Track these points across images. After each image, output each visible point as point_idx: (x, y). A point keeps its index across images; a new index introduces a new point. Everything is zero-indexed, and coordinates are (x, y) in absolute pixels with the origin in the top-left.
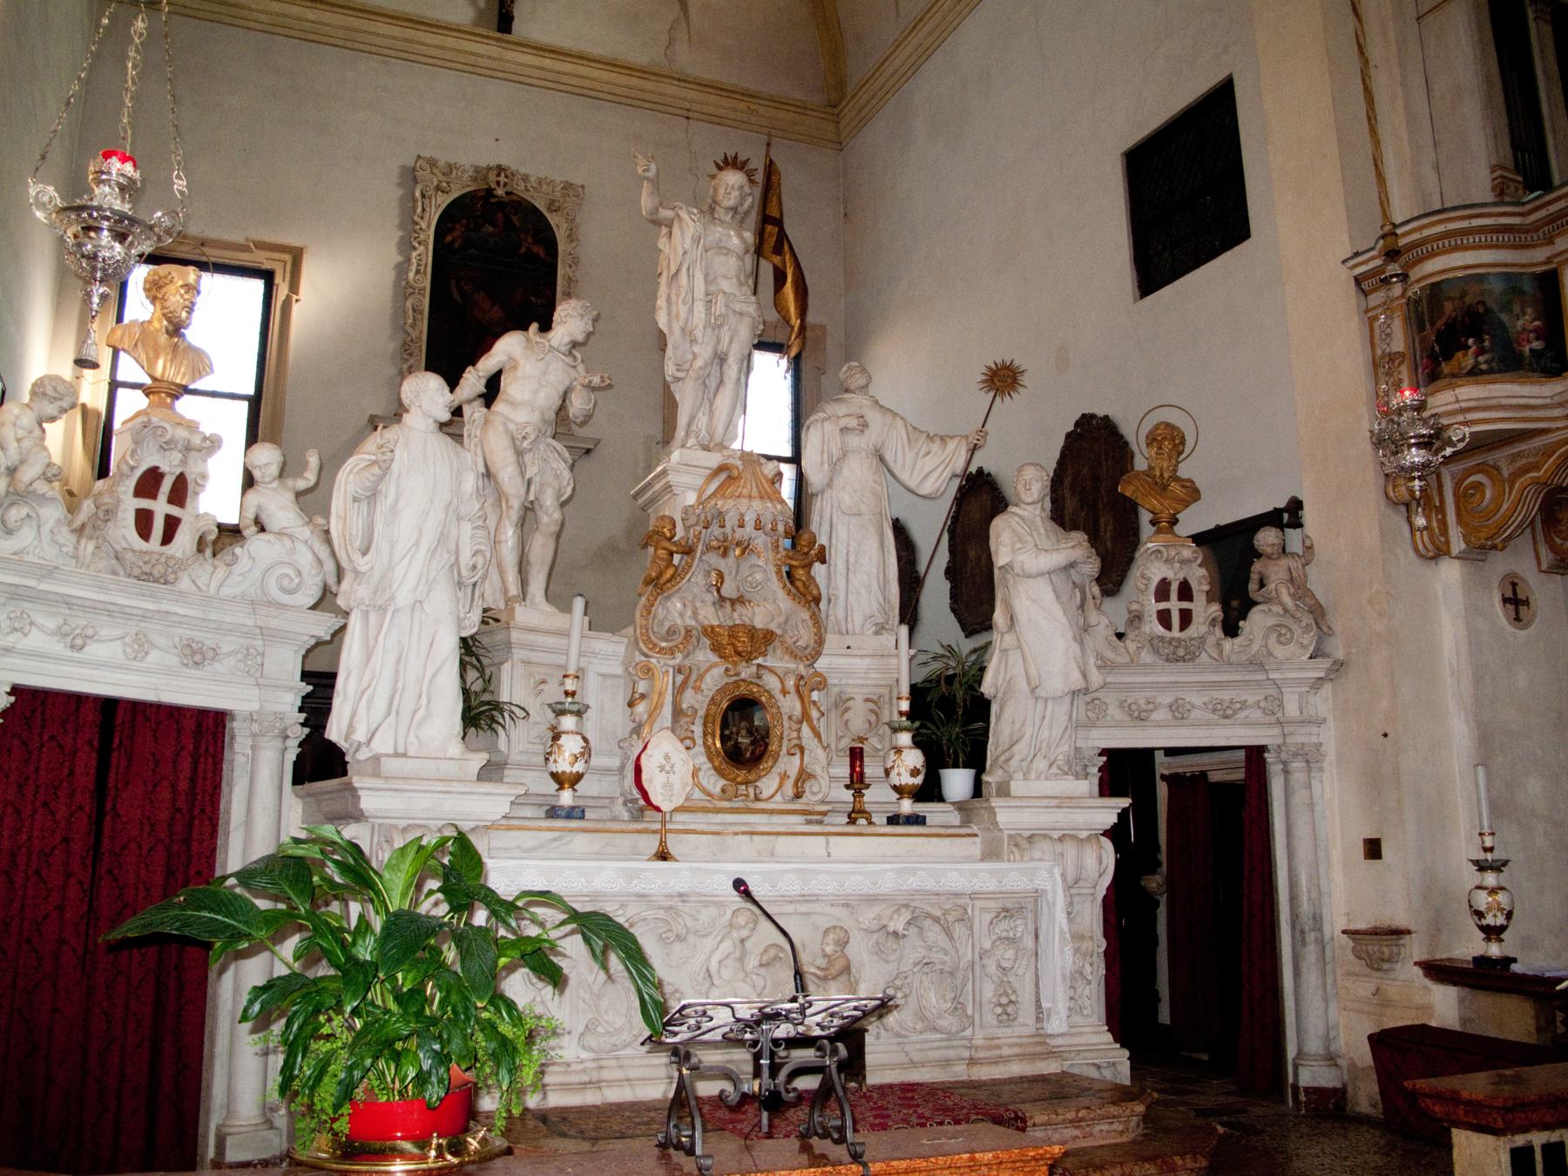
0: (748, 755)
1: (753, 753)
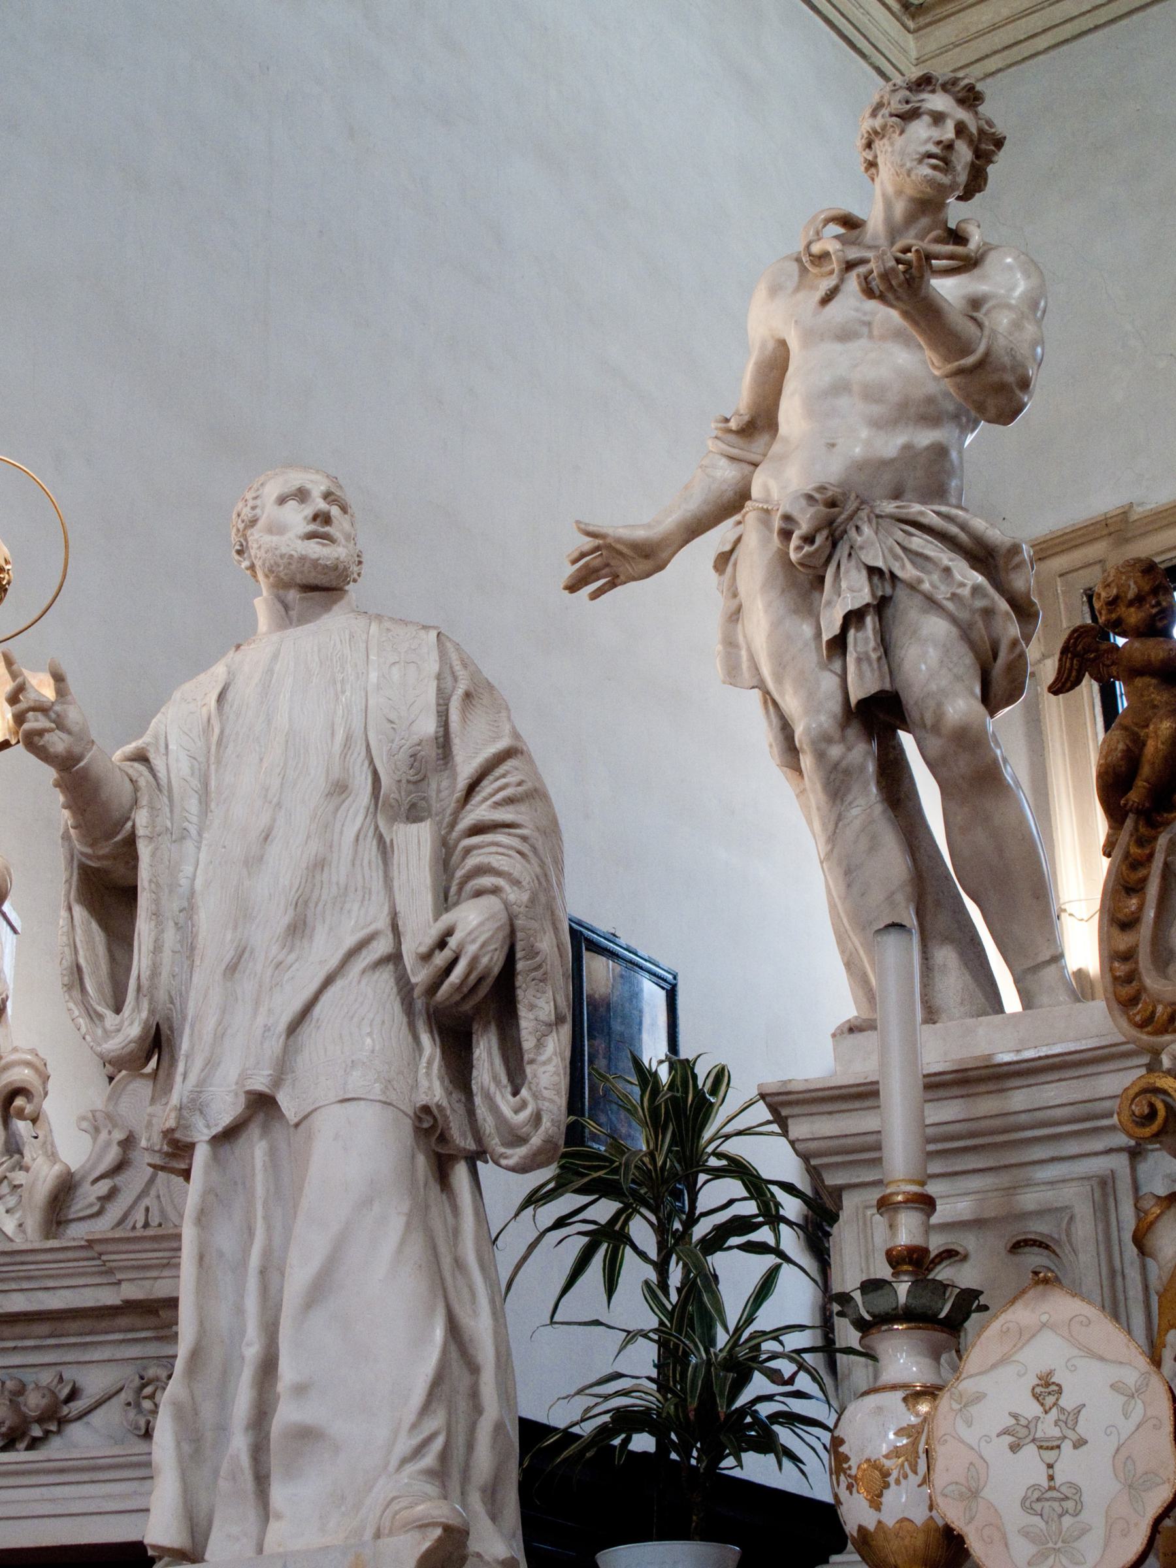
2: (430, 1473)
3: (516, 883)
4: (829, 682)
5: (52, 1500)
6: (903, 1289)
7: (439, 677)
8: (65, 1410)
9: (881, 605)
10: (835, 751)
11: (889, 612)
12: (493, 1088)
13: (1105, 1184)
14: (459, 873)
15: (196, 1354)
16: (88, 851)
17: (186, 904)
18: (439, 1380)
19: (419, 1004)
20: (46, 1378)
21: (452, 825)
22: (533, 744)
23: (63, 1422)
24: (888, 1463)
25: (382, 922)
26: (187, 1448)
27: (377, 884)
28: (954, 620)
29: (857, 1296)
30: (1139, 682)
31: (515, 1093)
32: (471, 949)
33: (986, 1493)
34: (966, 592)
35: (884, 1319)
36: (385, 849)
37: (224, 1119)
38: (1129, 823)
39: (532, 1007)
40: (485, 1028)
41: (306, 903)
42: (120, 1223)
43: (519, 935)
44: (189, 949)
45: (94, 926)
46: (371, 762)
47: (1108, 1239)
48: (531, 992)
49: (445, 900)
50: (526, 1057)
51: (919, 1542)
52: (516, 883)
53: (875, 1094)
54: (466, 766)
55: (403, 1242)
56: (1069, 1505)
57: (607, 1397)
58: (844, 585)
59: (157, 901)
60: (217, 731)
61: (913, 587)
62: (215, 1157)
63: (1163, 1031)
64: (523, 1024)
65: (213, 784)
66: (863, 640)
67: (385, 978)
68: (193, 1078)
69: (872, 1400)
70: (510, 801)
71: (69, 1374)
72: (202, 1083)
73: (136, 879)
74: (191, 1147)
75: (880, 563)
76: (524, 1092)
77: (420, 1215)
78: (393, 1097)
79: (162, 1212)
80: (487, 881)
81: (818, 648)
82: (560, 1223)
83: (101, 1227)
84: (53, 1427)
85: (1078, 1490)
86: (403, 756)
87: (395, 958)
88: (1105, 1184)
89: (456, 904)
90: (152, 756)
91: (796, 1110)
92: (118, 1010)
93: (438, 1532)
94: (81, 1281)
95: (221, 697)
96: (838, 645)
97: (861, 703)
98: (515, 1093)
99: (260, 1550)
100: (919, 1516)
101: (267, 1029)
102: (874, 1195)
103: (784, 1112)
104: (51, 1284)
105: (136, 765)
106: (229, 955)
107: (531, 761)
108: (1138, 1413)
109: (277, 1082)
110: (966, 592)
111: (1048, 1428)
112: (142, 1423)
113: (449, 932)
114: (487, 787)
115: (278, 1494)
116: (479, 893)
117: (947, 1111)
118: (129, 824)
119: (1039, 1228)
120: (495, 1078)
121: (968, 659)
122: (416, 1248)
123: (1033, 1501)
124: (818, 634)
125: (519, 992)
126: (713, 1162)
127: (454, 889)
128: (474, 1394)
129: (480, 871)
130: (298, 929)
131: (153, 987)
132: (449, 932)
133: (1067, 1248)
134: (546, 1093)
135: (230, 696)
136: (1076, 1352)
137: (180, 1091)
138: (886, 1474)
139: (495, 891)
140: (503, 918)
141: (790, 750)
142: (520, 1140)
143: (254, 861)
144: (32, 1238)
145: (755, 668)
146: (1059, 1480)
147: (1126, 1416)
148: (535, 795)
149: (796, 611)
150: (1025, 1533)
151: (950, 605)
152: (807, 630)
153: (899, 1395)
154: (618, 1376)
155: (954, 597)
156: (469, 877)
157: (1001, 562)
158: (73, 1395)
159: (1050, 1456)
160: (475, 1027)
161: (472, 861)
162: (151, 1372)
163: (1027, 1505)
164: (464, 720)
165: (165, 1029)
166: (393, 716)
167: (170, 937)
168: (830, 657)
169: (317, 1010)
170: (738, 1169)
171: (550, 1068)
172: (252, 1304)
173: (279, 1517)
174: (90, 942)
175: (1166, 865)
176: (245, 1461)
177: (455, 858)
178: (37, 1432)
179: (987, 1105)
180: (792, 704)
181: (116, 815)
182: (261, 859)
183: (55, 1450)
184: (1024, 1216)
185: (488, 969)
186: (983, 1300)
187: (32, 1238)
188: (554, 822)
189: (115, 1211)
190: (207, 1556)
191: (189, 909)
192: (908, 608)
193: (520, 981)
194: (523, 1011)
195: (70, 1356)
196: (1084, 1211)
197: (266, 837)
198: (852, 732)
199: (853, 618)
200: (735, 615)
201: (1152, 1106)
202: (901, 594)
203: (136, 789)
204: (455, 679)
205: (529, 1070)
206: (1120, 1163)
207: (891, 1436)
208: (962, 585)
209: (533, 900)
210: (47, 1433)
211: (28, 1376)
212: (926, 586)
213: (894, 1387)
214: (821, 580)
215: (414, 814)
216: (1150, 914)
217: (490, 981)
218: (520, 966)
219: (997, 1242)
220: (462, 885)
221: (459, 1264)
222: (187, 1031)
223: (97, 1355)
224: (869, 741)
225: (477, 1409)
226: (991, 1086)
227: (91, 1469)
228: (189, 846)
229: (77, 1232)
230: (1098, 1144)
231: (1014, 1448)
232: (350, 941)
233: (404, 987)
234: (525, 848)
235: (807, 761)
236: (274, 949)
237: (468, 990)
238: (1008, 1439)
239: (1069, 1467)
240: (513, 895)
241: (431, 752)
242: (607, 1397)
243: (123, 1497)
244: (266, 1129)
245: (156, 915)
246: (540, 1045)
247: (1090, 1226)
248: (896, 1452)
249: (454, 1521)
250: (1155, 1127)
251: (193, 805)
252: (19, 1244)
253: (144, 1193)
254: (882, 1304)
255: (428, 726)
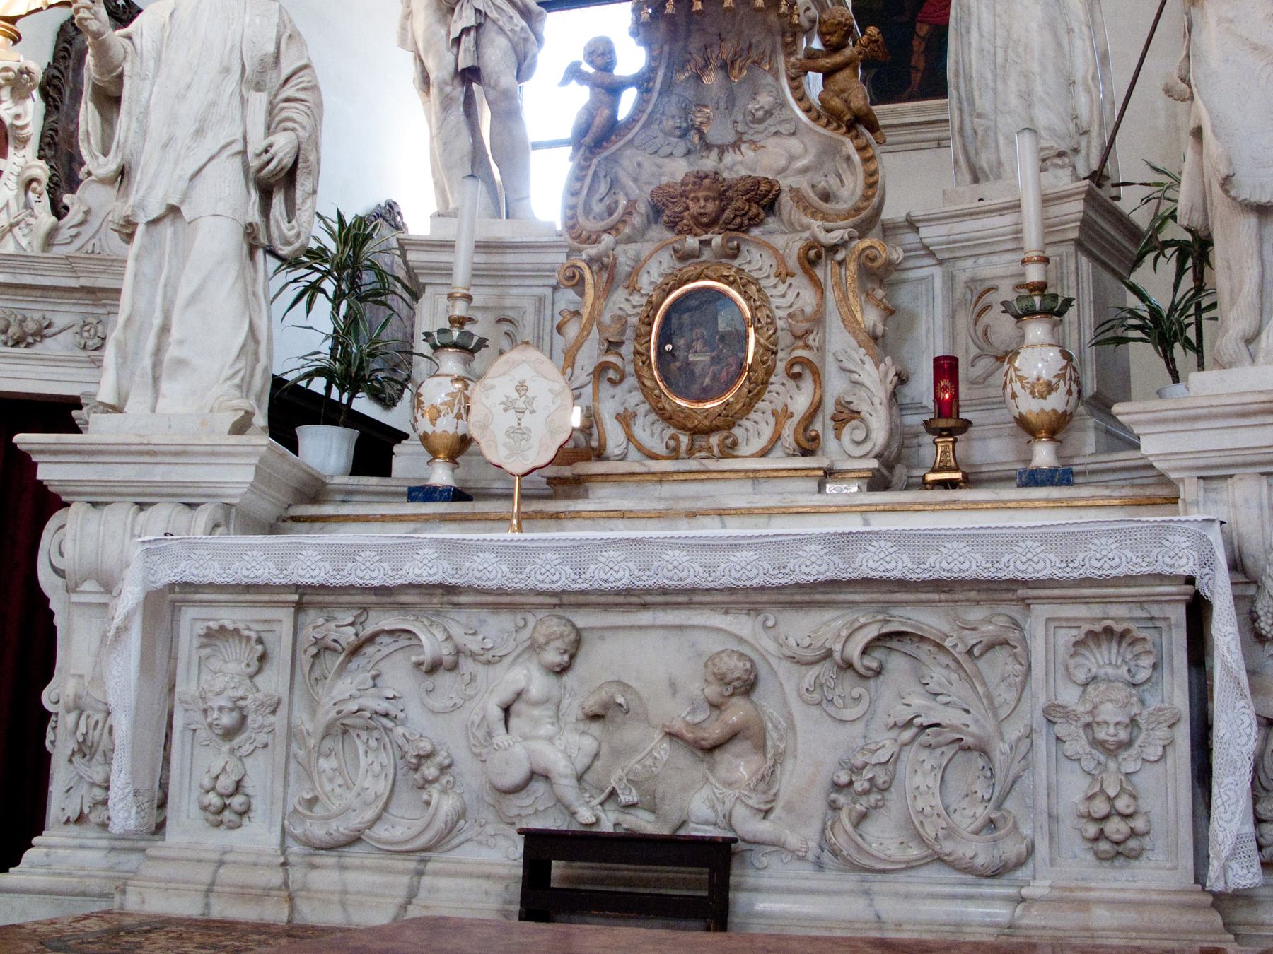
0: (707, 381)
1: (715, 377)
2: (239, 387)
3: (304, 128)
4: (450, 57)
5: (36, 372)
6: (456, 334)
7: (278, 25)
8: (45, 332)
9: (478, 27)
10: (448, 89)
11: (481, 31)
12: (280, 219)
13: (541, 300)
14: (277, 119)
15: (129, 320)
16: (98, 77)
17: (143, 110)
18: (244, 346)
19: (251, 176)
20: (37, 316)
21: (276, 95)
22: (315, 64)
23: (43, 337)
24: (441, 408)
25: (239, 136)
26: (120, 361)
27: (238, 117)
28: (511, 41)
29: (435, 334)
30: (597, 90)
31: (289, 222)
32: (281, 155)
33: (491, 427)
34: (518, 29)
35: (445, 346)
36: (244, 102)
37: (154, 215)
38: (582, 150)
39: (303, 185)
40: (280, 190)
41: (205, 121)
42: (79, 249)
43: (302, 152)
44: (144, 132)
45: (96, 113)
46: (242, 59)
47: (539, 324)
48: (303, 178)
49: (269, 130)
50: (297, 207)
51: (450, 441)
52: (304, 128)
53: (453, 246)
54: (286, 70)
55: (234, 284)
56: (525, 436)
57: (313, 361)
58: (464, 15)
59: (130, 107)
60: (168, 31)
61: (494, 22)
62: (147, 231)
63: (584, 242)
64: (297, 191)
65: (163, 57)
66: (468, 41)
67: (238, 161)
68: (141, 194)
69: (436, 380)
70: (304, 89)
71: (48, 315)
72: (144, 197)
73: (121, 92)
74: (136, 224)
75: (481, 8)
76: (294, 222)
77: (241, 274)
78: (236, 217)
79: (101, 246)
80: (290, 125)
81: (447, 43)
82: (296, 281)
83: (70, 250)
84: (38, 339)
85: (529, 430)
86: (256, 60)
87: (243, 153)
88: (541, 300)
89: (274, 133)
90: (134, 38)
91: (413, 248)
92: (105, 154)
93: (242, 413)
94: (60, 274)
95: (172, 15)
96: (457, 41)
97: (464, 70)
98: (289, 222)
99: (153, 410)
100: (451, 430)
101: (180, 177)
102: (446, 290)
103: (406, 247)
104: (44, 273)
105: (126, 40)
106: (165, 140)
107: (314, 71)
108: (558, 402)
109: (182, 202)
110: (518, 29)
111: (520, 404)
112: (83, 342)
113: (271, 146)
114: (294, 81)
115: (165, 386)
116: (285, 130)
117: (480, 258)
118: (120, 69)
119: (510, 314)
120: (281, 214)
121: (514, 59)
122: (240, 286)
123: (511, 433)
124: (448, 34)
125: (298, 177)
126: (366, 263)
127: (273, 126)
128: (256, 354)
129: (287, 119)
130: (199, 132)
131: (125, 147)
132: (271, 146)
133: (521, 324)
134: (304, 224)
135: (176, 15)
136: (535, 374)
137: (133, 199)
138: (439, 412)
139: (293, 130)
140: (296, 142)
141: (425, 80)
142: (288, 243)
143: (181, 97)
144: (36, 250)
145: (415, 43)
146: (521, 426)
147: (553, 403)
148: (314, 88)
149: (439, 22)
150: (505, 445)
151: (509, 33)
152: (443, 32)
153: (449, 379)
154: (318, 353)
155: (512, 30)
156: (281, 121)
157: (534, 16)
158: (48, 326)
159: (520, 415)
160: (275, 189)
161: (284, 114)
162: (89, 320)
163: (507, 434)
164: (287, 48)
165: (127, 167)
166: (255, 40)
167: (134, 125)
168: (452, 45)
169: (204, 171)
170: (374, 267)
171: (307, 213)
172: (159, 300)
173: (164, 396)
174: (94, 123)
175: (595, 171)
176: (149, 370)
177: (275, 112)
178: (30, 340)
179: (496, 259)
180: (430, 64)
181: (116, 63)
182: (184, 97)
183: (38, 349)
184: (505, 308)
185: (286, 164)
186: (487, 343)
187: (37, 252)
188: (321, 101)
189: (78, 243)
190: (126, 409)
191: (146, 113)
192: (490, 32)
193: (299, 172)
194: (298, 186)
195: (50, 307)
196: (531, 310)
197: (189, 86)
198: (457, 82)
199: (466, 31)
200: (408, 16)
201: (574, 273)
202: (488, 24)
203: (126, 53)
204: (285, 27)
205: (297, 213)
206: (548, 291)
207: (443, 395)
208: (516, 25)
209: (310, 136)
210: (35, 341)
211: (28, 314)
212: (500, 23)
213: (447, 375)
214: (453, 10)
215: (258, 87)
216: (585, 191)
217: (286, 170)
218: (300, 165)
219: (491, 317)
220: (276, 127)
221: (255, 294)
222: (140, 171)
223: (62, 308)
224: (463, 85)
225: (257, 360)
226: (499, 251)
227: (56, 361)
228: (148, 83)
229: (57, 251)
230: (541, 282)
231: (505, 410)
232: (223, 142)
233: (246, 167)
234: (309, 113)
235: (434, 91)
236: (187, 140)
237: (274, 174)
238: (504, 406)
239: (527, 420)
240: (301, 133)
241: (271, 60)
242: (313, 361)
243: (71, 375)
244: (173, 223)
245: (129, 114)
246: (303, 202)
247: (532, 317)
248: (445, 403)
249: (250, 410)
250: (575, 281)
251: (151, 64)
252: (29, 252)
253: (93, 237)
254: (446, 340)
255: (271, 48)
